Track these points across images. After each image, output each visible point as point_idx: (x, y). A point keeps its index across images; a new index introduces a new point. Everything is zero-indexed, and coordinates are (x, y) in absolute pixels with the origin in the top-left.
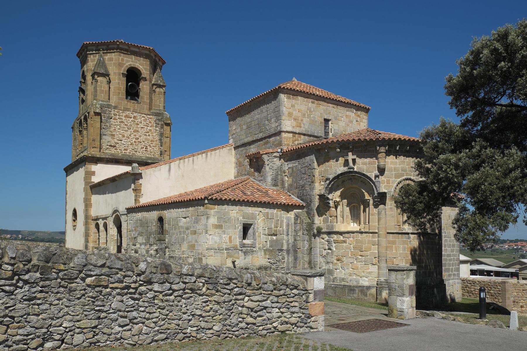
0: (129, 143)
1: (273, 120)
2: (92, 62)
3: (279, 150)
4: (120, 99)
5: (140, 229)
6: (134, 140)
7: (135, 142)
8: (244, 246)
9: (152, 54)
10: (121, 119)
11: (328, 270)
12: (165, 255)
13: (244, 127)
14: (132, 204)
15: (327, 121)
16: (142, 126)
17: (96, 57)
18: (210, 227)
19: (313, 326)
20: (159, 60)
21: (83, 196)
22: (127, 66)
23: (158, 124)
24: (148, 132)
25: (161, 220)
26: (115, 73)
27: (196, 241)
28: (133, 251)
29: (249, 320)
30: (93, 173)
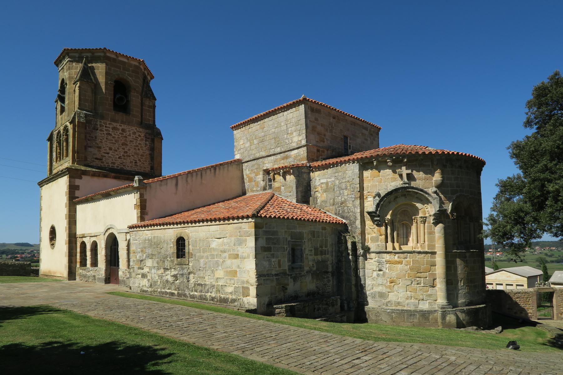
0: (117, 156)
1: (295, 134)
5: (149, 251)
9: (141, 67)
12: (188, 281)
13: (256, 142)
20: (148, 74)
23: (148, 138)
24: (137, 146)
25: (181, 243)
27: (238, 267)
28: (140, 276)
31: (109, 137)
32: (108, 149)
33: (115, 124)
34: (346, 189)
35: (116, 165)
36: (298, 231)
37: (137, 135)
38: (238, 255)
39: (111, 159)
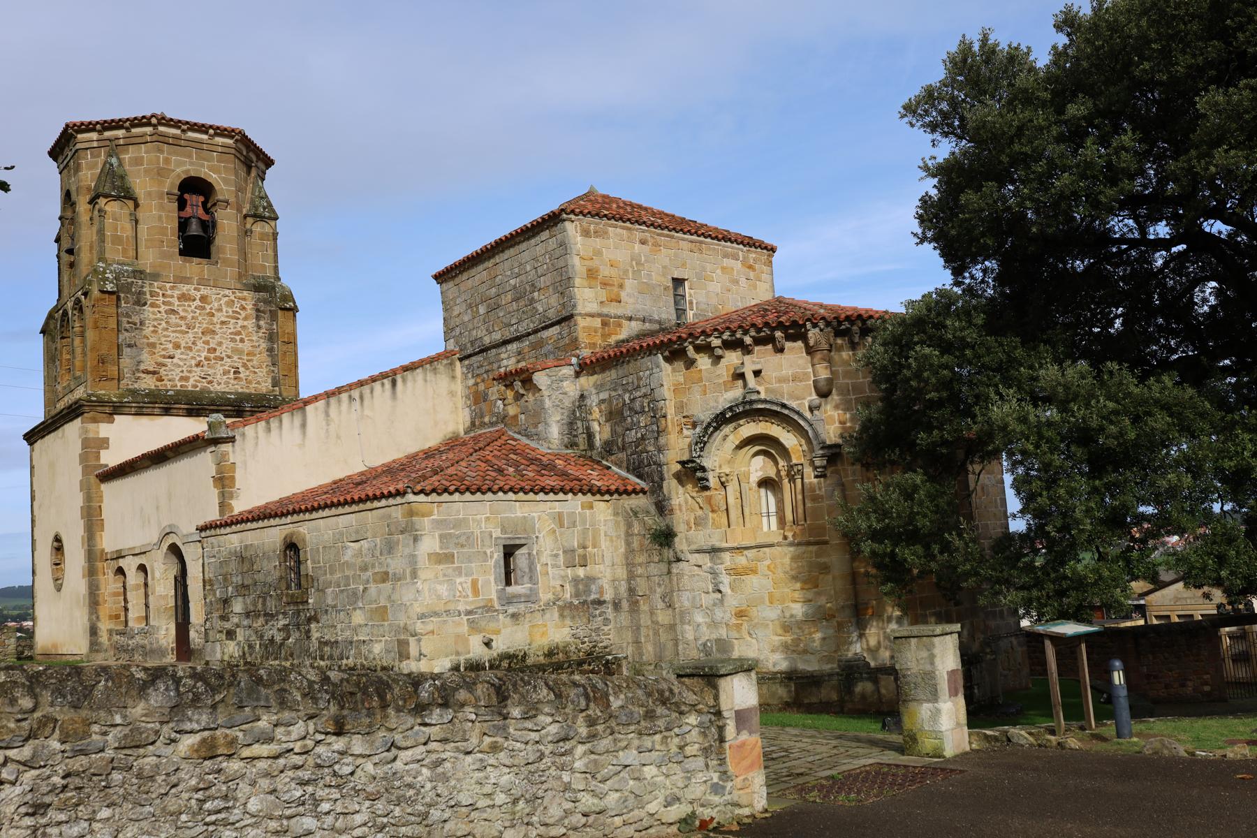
0: (193, 362)
2: (90, 169)
3: (574, 360)
4: (164, 255)
6: (204, 354)
7: (207, 359)
8: (509, 600)
10: (169, 303)
11: (718, 641)
13: (482, 310)
14: (213, 515)
15: (678, 282)
16: (223, 319)
17: (99, 156)
18: (423, 560)
19: (743, 801)
21: (78, 500)
22: (179, 175)
23: (263, 312)
24: (239, 333)
25: (292, 547)
26: (149, 194)
29: (587, 801)
30: (104, 443)
31: (173, 319)
32: (170, 346)
33: (185, 288)
34: (643, 412)
35: (191, 381)
36: (519, 514)
37: (237, 307)
38: (387, 573)
39: (178, 370)
